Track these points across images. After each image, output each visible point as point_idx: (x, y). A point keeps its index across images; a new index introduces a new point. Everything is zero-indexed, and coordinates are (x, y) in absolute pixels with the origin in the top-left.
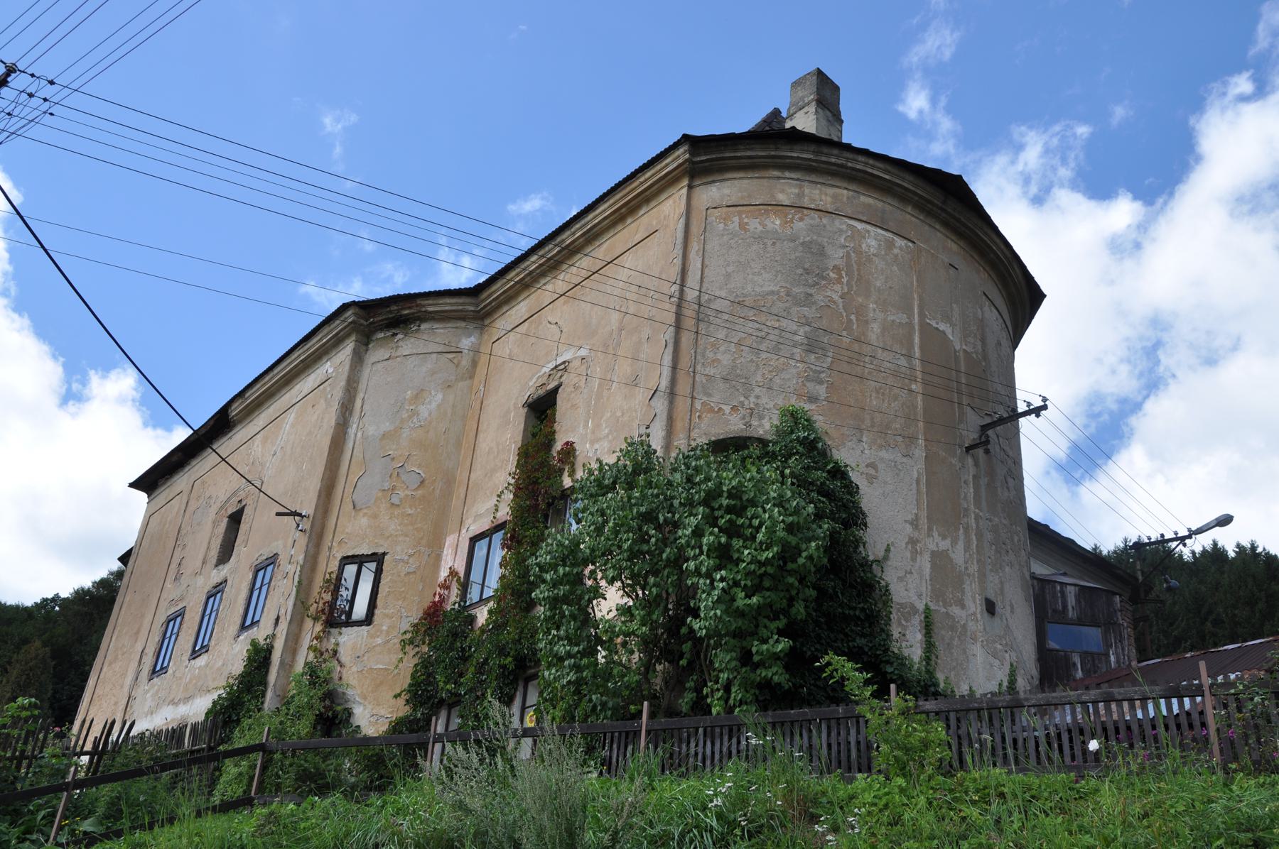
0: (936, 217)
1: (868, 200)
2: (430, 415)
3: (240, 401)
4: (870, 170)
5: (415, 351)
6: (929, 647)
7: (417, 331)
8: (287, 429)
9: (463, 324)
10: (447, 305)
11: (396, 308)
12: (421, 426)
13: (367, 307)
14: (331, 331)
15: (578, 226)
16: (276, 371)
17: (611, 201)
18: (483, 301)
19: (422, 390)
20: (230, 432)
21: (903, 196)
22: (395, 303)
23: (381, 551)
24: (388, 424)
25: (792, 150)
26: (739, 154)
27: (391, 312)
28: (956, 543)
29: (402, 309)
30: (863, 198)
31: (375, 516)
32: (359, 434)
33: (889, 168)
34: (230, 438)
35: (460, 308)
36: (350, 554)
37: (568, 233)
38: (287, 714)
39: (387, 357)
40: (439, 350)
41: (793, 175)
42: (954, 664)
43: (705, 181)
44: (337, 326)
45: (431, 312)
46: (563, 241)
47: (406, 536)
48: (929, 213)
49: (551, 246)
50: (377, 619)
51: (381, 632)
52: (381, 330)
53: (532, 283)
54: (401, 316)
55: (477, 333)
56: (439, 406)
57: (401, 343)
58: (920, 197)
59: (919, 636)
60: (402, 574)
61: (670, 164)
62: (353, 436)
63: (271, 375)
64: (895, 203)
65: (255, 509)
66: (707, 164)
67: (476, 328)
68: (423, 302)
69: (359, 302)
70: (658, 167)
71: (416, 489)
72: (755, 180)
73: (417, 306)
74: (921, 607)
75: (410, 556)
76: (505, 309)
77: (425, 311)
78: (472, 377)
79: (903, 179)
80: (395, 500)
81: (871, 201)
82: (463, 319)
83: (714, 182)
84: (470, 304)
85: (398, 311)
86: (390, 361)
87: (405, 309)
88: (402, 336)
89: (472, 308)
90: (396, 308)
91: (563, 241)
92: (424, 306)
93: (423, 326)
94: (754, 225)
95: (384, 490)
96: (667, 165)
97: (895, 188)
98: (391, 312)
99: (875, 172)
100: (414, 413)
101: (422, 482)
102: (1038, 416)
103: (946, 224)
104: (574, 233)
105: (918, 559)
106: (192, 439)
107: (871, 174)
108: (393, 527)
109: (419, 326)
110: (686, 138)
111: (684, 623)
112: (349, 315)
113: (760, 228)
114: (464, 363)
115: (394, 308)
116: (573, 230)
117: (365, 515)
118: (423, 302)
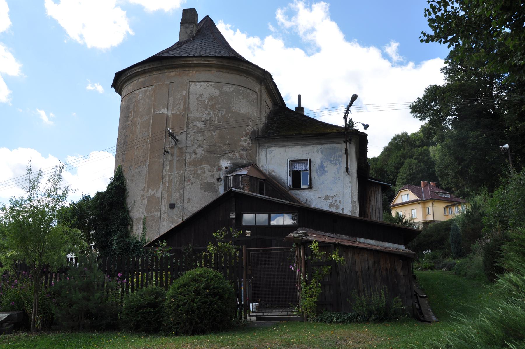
0: (163, 69)
1: (141, 79)
4: (136, 71)
6: (144, 230)
21: (150, 71)
28: (158, 190)
30: (140, 80)
33: (140, 67)
38: (16, 278)
41: (126, 84)
42: (153, 231)
48: (160, 70)
50: (314, 185)
58: (153, 68)
59: (142, 227)
64: (149, 74)
74: (143, 217)
79: (145, 67)
81: (142, 79)
97: (146, 71)
99: (138, 71)
103: (168, 69)
105: (144, 201)
107: (137, 72)
111: (510, 131)
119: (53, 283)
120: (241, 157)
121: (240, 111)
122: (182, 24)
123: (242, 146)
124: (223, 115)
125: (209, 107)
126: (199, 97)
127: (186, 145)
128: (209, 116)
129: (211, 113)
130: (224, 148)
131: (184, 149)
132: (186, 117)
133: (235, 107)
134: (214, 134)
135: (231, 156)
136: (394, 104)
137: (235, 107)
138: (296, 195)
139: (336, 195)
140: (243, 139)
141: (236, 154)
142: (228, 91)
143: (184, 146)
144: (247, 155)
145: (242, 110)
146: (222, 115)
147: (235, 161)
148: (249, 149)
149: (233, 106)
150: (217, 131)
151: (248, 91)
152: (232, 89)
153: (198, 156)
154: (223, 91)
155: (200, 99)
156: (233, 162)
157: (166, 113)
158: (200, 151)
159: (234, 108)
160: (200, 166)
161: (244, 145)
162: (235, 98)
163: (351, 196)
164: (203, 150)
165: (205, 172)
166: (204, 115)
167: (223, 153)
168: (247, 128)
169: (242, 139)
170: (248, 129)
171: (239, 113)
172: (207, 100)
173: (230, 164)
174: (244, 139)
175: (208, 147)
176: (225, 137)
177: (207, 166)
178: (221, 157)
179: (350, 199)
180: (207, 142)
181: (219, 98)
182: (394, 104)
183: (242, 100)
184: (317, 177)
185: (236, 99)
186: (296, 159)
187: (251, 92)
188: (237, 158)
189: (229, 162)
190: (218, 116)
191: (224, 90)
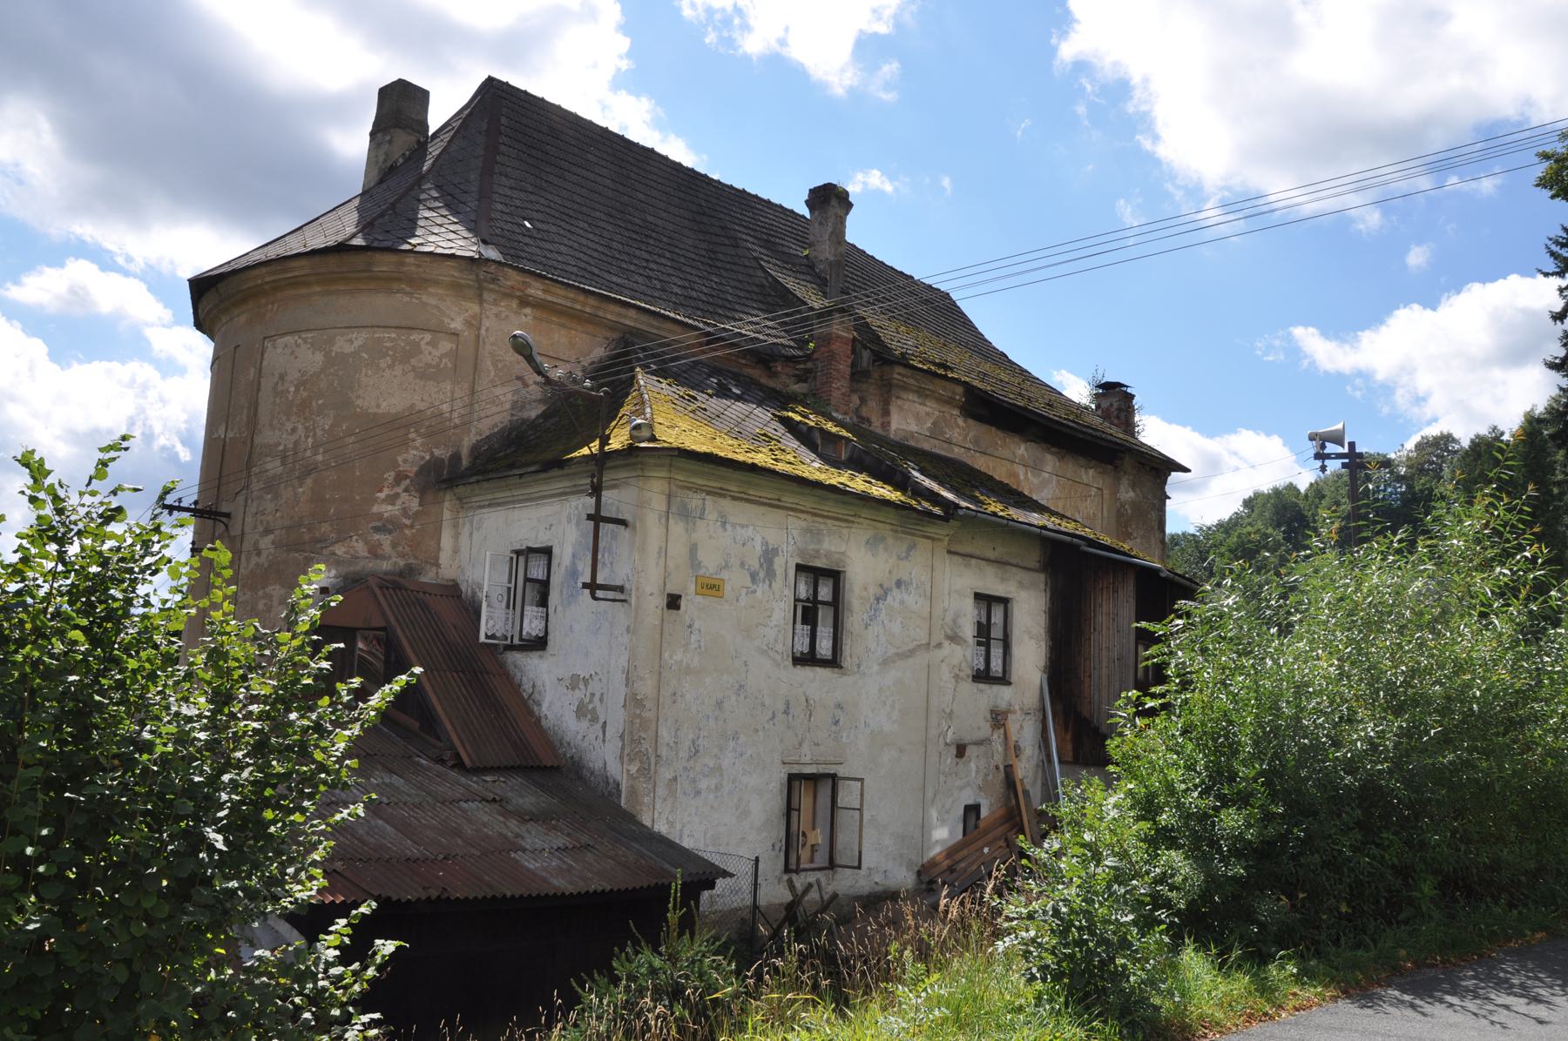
119: (183, 824)
120: (374, 552)
121: (378, 406)
122: (372, 134)
123: (380, 516)
124: (327, 427)
125: (295, 409)
126: (277, 383)
127: (243, 530)
128: (293, 438)
129: (300, 426)
130: (323, 529)
131: (238, 539)
132: (249, 445)
133: (364, 398)
134: (300, 490)
135: (339, 552)
136: (967, 272)
137: (364, 398)
138: (515, 666)
139: (593, 673)
140: (382, 495)
141: (356, 544)
142: (348, 349)
143: (239, 533)
144: (394, 545)
145: (384, 404)
146: (323, 429)
147: (352, 569)
148: (407, 522)
149: (358, 397)
150: (309, 482)
151: (415, 336)
152: (357, 343)
153: (263, 559)
154: (333, 354)
155: (280, 388)
156: (344, 570)
157: (223, 436)
158: (266, 543)
159: (359, 402)
160: (263, 588)
161: (386, 515)
162: (364, 370)
163: (627, 679)
164: (273, 543)
165: (271, 606)
166: (284, 436)
167: (319, 546)
168: (400, 459)
169: (379, 494)
170: (405, 461)
171: (376, 414)
172: (292, 389)
173: (335, 577)
174: (387, 496)
175: (284, 531)
176: (327, 496)
177: (278, 587)
178: (312, 559)
179: (623, 690)
180: (282, 518)
181: (323, 376)
182: (967, 272)
183: (387, 373)
184: (560, 608)
185: (370, 372)
186: (762, 509)
187: (428, 337)
188: (358, 558)
189: (333, 572)
190: (315, 435)
191: (336, 349)
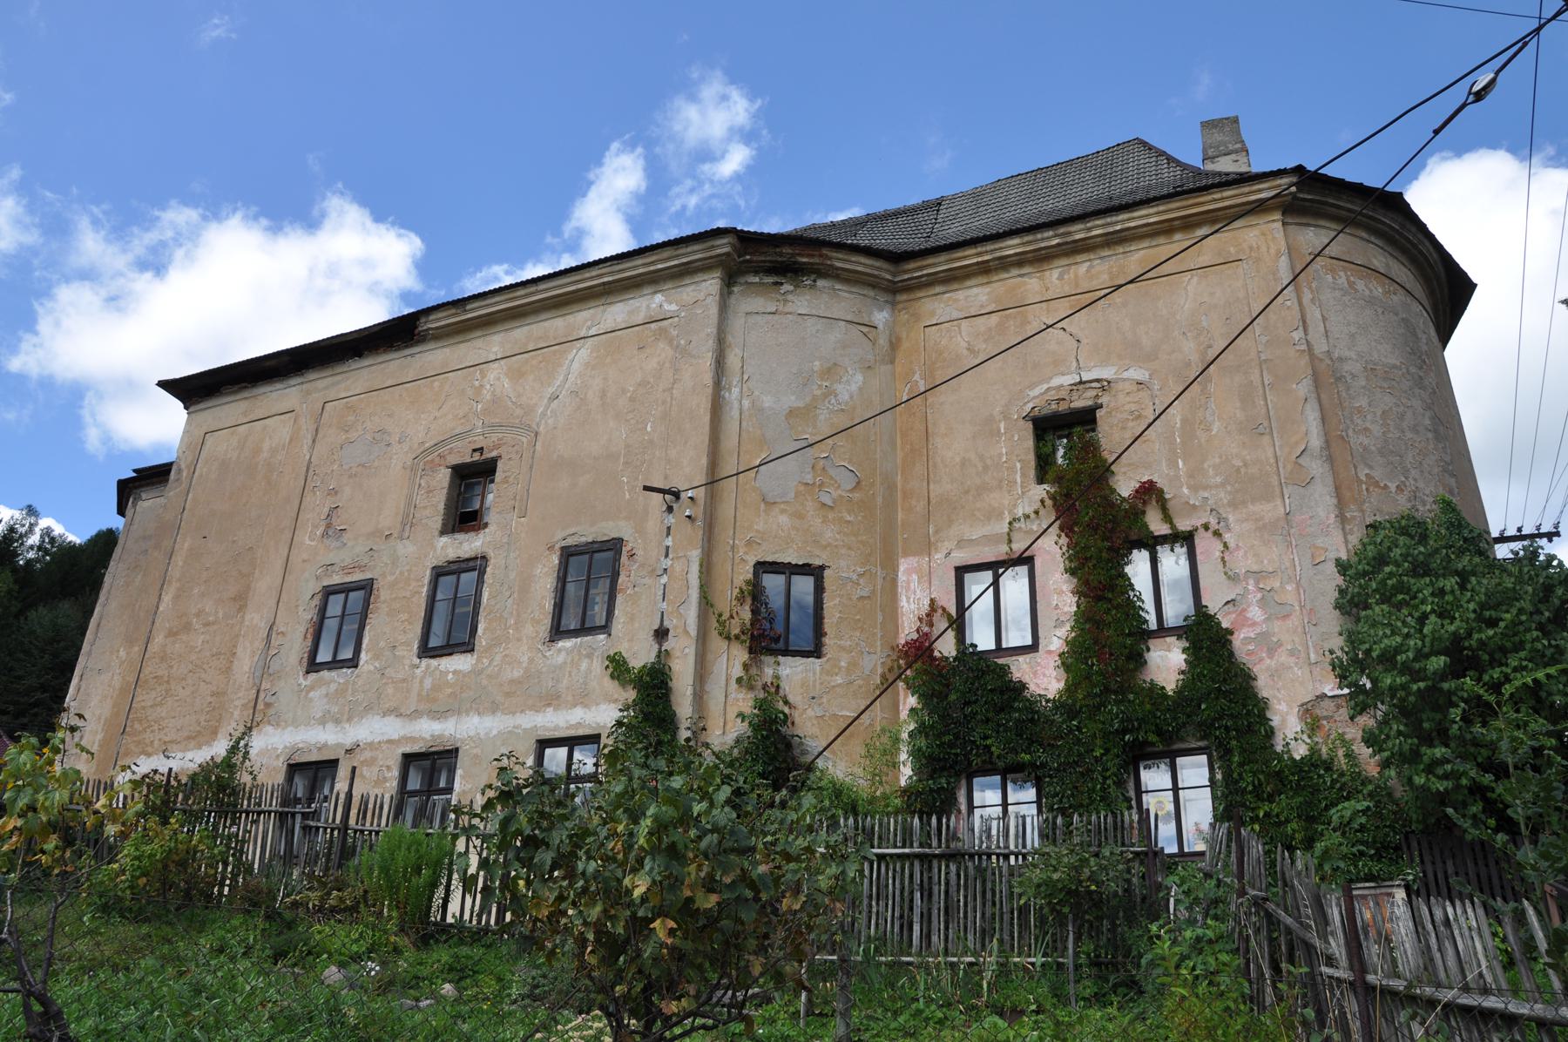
2: (851, 397)
3: (453, 311)
5: (814, 312)
7: (812, 287)
8: (576, 365)
9: (871, 293)
10: (861, 264)
11: (790, 251)
12: (842, 410)
13: (748, 241)
14: (677, 257)
15: (1098, 222)
16: (542, 286)
17: (1161, 208)
18: (906, 272)
19: (835, 364)
20: (407, 347)
22: (791, 245)
23: (817, 562)
24: (793, 398)
25: (1385, 216)
26: (1341, 204)
27: (781, 254)
29: (799, 255)
31: (799, 516)
32: (746, 403)
34: (412, 355)
35: (876, 273)
36: (769, 559)
37: (1080, 226)
39: (774, 310)
40: (849, 318)
41: (1377, 241)
43: (1297, 220)
44: (695, 253)
45: (838, 269)
46: (1069, 233)
47: (850, 548)
49: (1051, 233)
51: (840, 668)
52: (756, 273)
53: (996, 269)
54: (795, 263)
55: (888, 308)
56: (860, 389)
57: (790, 297)
60: (855, 598)
61: (1265, 191)
62: (736, 405)
63: (532, 289)
65: (531, 467)
66: (1307, 204)
67: (887, 302)
68: (830, 254)
69: (742, 231)
70: (1246, 189)
71: (851, 491)
72: (1357, 240)
73: (821, 256)
75: (860, 575)
76: (938, 289)
77: (831, 266)
78: (892, 362)
80: (827, 500)
82: (873, 286)
83: (1308, 225)
84: (887, 271)
85: (793, 255)
86: (776, 317)
87: (802, 256)
88: (791, 288)
89: (888, 277)
90: (790, 251)
91: (1069, 233)
92: (830, 259)
93: (821, 283)
94: (1360, 285)
95: (807, 484)
96: (1260, 191)
98: (781, 254)
100: (829, 393)
101: (858, 483)
102: (1550, 541)
104: (1090, 229)
106: (334, 341)
108: (829, 534)
109: (815, 281)
110: (1299, 170)
112: (723, 246)
113: (1367, 292)
114: (881, 341)
115: (787, 250)
116: (1089, 225)
117: (783, 511)
118: (830, 254)
